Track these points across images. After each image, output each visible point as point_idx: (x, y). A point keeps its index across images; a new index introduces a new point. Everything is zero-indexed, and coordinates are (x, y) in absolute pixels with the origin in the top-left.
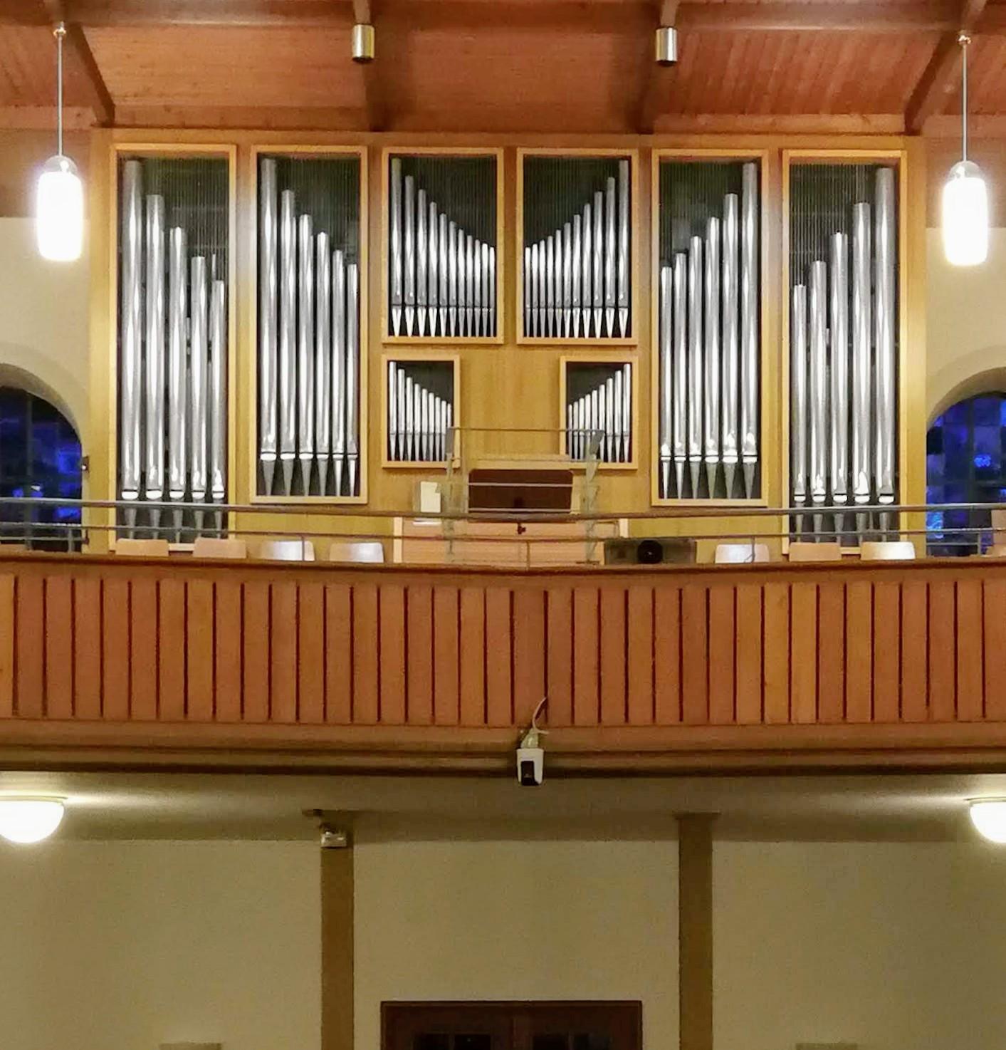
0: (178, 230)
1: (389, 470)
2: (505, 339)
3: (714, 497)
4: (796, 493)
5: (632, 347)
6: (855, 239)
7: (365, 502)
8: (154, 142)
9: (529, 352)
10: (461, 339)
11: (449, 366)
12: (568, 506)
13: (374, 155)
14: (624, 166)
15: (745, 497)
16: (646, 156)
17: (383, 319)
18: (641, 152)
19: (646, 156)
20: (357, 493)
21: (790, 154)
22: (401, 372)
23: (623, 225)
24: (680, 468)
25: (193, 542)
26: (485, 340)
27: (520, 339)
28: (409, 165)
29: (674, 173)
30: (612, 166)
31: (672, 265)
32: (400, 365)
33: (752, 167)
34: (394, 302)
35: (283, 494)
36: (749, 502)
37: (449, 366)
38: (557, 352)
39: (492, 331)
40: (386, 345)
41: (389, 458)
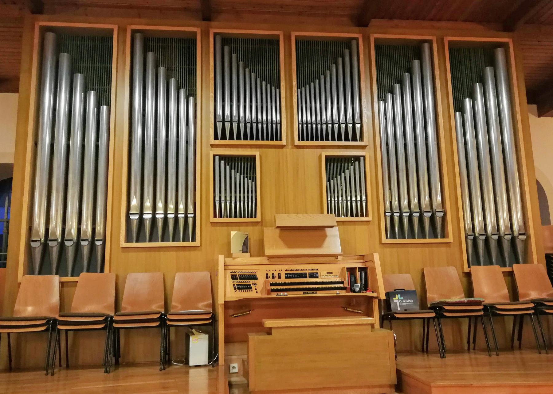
0: (173, 79)
1: (213, 224)
2: (287, 142)
3: (418, 238)
4: (169, 212)
5: (363, 147)
6: (486, 86)
7: (199, 245)
8: (153, 25)
9: (301, 150)
10: (260, 142)
11: (252, 159)
12: (533, 263)
13: (205, 34)
14: (354, 43)
15: (437, 238)
16: (367, 39)
17: (211, 129)
18: (119, 28)
19: (367, 39)
20: (193, 239)
21: (294, 34)
22: (222, 162)
23: (427, 81)
24: (406, 220)
25: (78, 276)
26: (274, 143)
27: (297, 142)
28: (225, 40)
29: (384, 50)
30: (348, 43)
31: (385, 101)
32: (222, 158)
33: (426, 46)
34: (218, 119)
35: (157, 241)
36: (439, 240)
37: (252, 159)
38: (319, 151)
39: (278, 137)
40: (212, 146)
41: (215, 216)
